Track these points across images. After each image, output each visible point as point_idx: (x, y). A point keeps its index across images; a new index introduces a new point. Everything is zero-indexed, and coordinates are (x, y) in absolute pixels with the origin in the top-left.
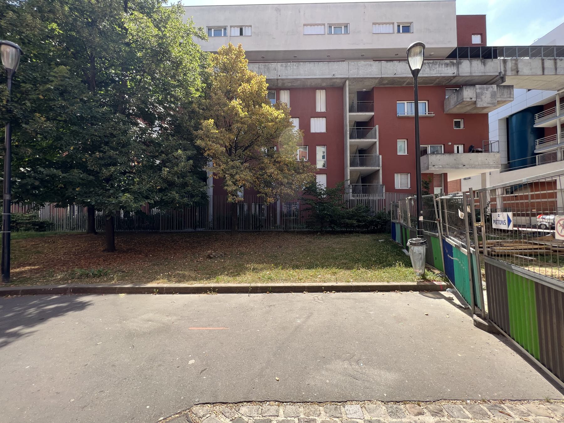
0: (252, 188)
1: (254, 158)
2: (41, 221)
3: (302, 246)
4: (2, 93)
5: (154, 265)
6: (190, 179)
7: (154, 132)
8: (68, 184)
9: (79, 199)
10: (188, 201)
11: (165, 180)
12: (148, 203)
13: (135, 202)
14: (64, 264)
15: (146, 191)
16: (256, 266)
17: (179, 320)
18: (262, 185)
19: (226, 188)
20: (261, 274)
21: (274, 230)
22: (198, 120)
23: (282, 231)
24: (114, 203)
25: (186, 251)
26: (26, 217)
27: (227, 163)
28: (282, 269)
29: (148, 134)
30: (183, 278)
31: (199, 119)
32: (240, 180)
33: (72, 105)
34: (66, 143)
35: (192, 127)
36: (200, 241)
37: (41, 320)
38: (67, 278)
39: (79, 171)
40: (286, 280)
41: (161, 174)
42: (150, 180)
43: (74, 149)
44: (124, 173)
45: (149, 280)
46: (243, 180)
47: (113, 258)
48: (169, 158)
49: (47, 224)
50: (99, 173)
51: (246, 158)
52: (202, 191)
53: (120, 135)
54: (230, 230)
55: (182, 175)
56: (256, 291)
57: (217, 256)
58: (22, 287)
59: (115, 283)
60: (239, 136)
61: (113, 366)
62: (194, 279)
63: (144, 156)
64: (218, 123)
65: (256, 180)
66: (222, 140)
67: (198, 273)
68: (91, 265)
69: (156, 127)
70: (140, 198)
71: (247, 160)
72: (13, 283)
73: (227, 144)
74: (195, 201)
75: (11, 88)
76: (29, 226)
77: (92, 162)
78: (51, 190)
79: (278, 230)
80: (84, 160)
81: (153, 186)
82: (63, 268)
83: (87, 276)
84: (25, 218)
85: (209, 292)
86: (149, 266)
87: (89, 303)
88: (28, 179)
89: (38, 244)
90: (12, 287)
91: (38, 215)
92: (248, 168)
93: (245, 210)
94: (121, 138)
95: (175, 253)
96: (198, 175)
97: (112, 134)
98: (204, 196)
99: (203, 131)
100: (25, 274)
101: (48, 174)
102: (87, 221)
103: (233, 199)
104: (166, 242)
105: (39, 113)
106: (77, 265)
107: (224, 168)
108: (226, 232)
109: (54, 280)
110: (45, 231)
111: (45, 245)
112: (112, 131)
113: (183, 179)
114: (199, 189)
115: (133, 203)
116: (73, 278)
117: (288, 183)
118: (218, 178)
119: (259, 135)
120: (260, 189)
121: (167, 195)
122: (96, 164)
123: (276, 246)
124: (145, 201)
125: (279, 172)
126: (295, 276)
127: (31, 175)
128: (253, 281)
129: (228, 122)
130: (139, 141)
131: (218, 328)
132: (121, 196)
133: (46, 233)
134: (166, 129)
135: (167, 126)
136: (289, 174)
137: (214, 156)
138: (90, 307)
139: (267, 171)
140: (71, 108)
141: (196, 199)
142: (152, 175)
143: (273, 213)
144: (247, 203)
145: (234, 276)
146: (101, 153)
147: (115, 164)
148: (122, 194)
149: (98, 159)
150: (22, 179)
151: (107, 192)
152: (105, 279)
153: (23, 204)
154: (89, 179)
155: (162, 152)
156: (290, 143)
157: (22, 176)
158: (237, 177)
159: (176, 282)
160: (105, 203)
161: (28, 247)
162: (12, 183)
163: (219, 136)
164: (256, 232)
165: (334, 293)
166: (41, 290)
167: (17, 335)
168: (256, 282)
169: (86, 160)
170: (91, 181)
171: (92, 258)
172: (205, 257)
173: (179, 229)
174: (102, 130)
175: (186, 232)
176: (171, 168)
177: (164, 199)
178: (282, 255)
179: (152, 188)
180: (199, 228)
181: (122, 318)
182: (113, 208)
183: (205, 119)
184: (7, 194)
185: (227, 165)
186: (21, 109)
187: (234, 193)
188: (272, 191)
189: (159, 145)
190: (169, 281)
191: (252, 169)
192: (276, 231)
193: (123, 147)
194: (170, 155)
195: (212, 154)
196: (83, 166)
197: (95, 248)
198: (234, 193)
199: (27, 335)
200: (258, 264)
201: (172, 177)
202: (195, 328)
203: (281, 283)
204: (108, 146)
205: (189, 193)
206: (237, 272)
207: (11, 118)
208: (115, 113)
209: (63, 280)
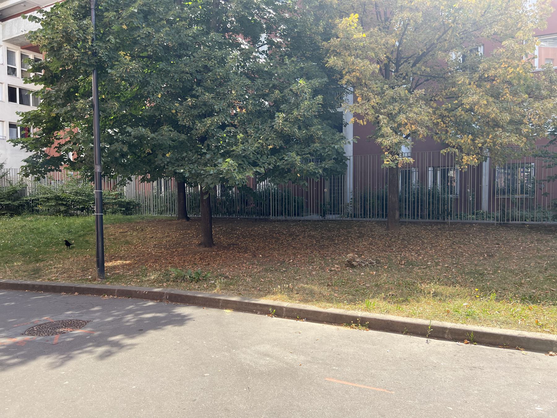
0: (429, 138)
1: (434, 77)
2: (127, 200)
3: (545, 256)
4: (87, 31)
5: (266, 270)
6: (318, 129)
7: (261, 54)
8: (157, 148)
9: (170, 169)
10: (314, 167)
11: (281, 135)
12: (257, 172)
13: (239, 172)
14: (155, 260)
15: (253, 153)
16: (440, 289)
17: (310, 362)
18: (452, 131)
19: (379, 140)
20: (451, 305)
21: (475, 221)
22: (330, 21)
23: (493, 224)
24: (211, 175)
25: (312, 252)
26: (112, 195)
27: (381, 93)
28: (497, 300)
29: (253, 59)
30: (310, 296)
31: (331, 17)
32: (406, 124)
33: (158, 31)
34: (154, 89)
35: (320, 35)
36: (333, 237)
37: (140, 332)
38: (162, 279)
39: (170, 129)
40: (506, 323)
41: (273, 124)
42: (258, 135)
43: (162, 96)
44: (223, 127)
45: (262, 293)
46: (411, 124)
47: (211, 256)
48: (285, 96)
49: (133, 206)
50: (192, 129)
51: (417, 78)
52: (337, 150)
53: (216, 67)
54: (384, 219)
55: (305, 124)
56: (441, 336)
57: (363, 265)
58: (117, 286)
59: (217, 293)
60: (405, 37)
61: (226, 409)
62: (328, 300)
63: (249, 96)
64: (365, 19)
65: (439, 120)
66: (373, 49)
67: (334, 291)
68: (186, 264)
69: (264, 44)
70: (245, 165)
71: (420, 82)
72: (108, 280)
73: (383, 57)
74: (326, 166)
75: (95, 22)
76: (115, 207)
77: (183, 113)
78: (138, 158)
79: (485, 221)
80: (174, 111)
81: (262, 145)
82: (156, 266)
83: (184, 279)
84: (111, 197)
85: (354, 325)
86: (259, 272)
87: (189, 317)
88: (116, 144)
89: (126, 232)
90: (108, 286)
91: (124, 193)
92: (422, 99)
93: (414, 182)
94: (218, 71)
95: (294, 254)
96: (330, 121)
97: (206, 67)
98: (340, 158)
99: (339, 40)
100: (117, 269)
101: (136, 136)
102: (176, 201)
103: (393, 161)
104: (280, 236)
105: (123, 51)
106: (170, 263)
107: (377, 103)
108: (377, 222)
109: (148, 280)
110: (131, 214)
111: (134, 234)
112: (205, 63)
113: (307, 129)
114: (333, 146)
115: (237, 174)
116: (168, 281)
117: (511, 122)
118: (365, 123)
119: (447, 29)
120: (447, 138)
121: (283, 159)
122: (188, 116)
123: (482, 254)
124: (252, 169)
125: (491, 99)
126: (527, 317)
127: (119, 138)
128: (436, 317)
129: (382, 13)
130: (241, 72)
131: (374, 389)
132: (221, 163)
133: (133, 216)
134: (278, 46)
135: (280, 40)
136: (514, 102)
137: (358, 84)
138: (190, 323)
139: (465, 101)
140: (156, 36)
141: (328, 164)
142: (260, 127)
143: (473, 187)
144: (418, 167)
145: (398, 302)
146: (194, 99)
147: (210, 114)
148: (222, 159)
149: (190, 107)
150: (110, 144)
151: (203, 158)
152: (205, 286)
153: (108, 178)
154: (181, 140)
155: (274, 87)
156: (520, 34)
157: (110, 140)
158: (402, 118)
159: (301, 301)
160: (201, 175)
161: (117, 235)
162: (102, 150)
163: (366, 43)
164: (437, 224)
165: (468, 343)
166: (136, 292)
167: (119, 346)
168: (442, 319)
169: (176, 112)
170: (182, 143)
171: (187, 254)
172: (344, 265)
173: (298, 215)
174: (193, 63)
175: (310, 221)
176: (288, 113)
177: (278, 166)
178: (495, 272)
179: (261, 149)
180: (331, 214)
181: (230, 345)
182: (211, 182)
183: (341, 17)
184: (98, 165)
185: (382, 97)
186: (106, 48)
187: (394, 151)
188: (473, 140)
189: (270, 74)
190: (291, 298)
191: (431, 100)
192: (480, 224)
193: (221, 85)
194: (286, 91)
195: (354, 80)
196: (174, 123)
197: (188, 240)
198: (394, 151)
199: (128, 347)
200: (443, 285)
201: (289, 127)
202: (335, 381)
203: (495, 328)
204: (201, 86)
205: (316, 154)
206: (402, 295)
207: (97, 62)
208: (208, 33)
209: (158, 281)
